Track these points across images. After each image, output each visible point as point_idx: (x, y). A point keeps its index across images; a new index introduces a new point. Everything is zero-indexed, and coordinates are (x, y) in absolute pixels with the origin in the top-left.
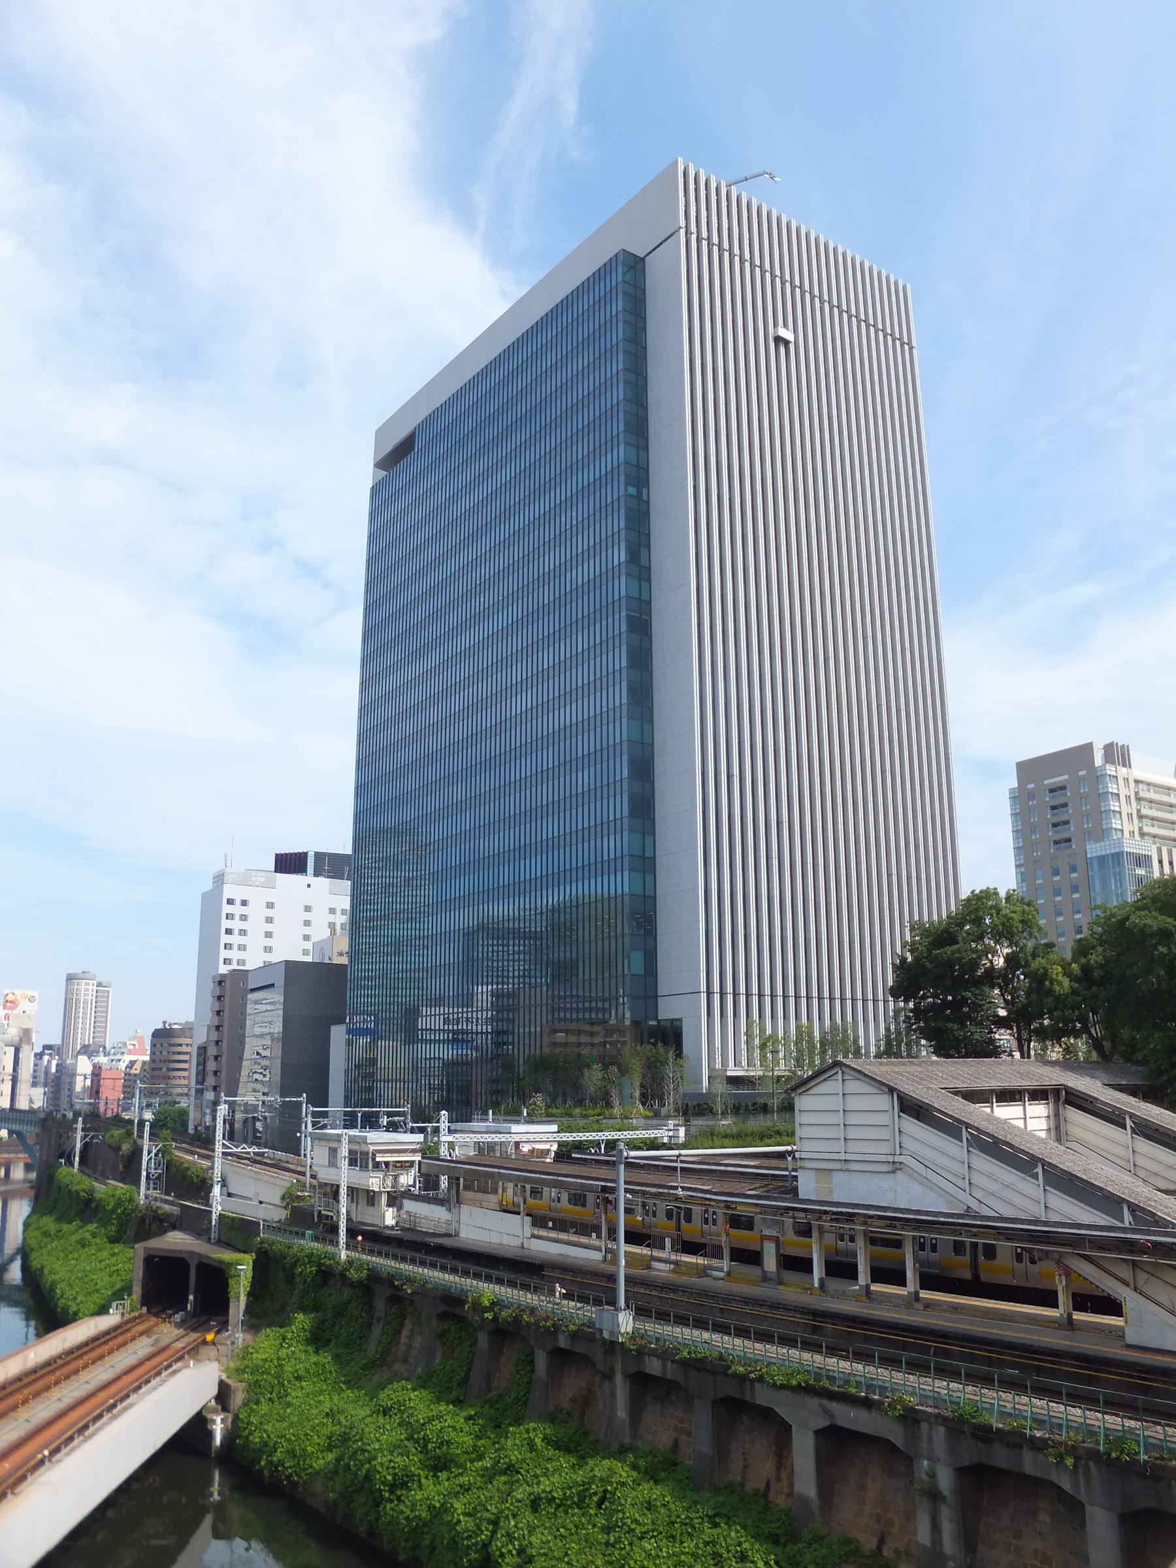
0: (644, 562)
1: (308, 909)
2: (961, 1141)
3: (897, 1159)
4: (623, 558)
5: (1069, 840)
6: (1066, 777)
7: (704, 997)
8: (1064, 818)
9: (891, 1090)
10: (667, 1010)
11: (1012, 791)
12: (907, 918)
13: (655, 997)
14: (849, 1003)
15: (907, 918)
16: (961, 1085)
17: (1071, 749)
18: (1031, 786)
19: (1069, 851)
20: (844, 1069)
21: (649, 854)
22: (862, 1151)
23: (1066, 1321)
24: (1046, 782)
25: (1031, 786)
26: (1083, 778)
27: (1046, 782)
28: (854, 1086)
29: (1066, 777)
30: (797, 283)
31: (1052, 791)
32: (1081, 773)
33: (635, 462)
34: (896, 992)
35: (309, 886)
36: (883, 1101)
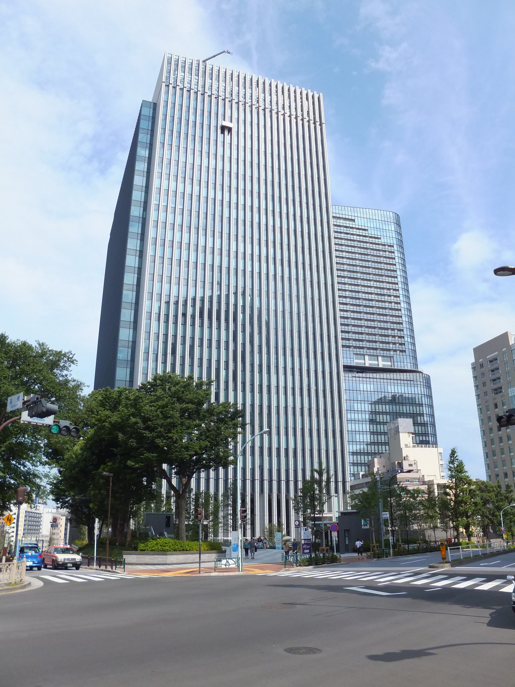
6: (497, 353)
8: (497, 375)
11: (473, 364)
12: (300, 477)
15: (300, 477)
16: (434, 656)
17: (498, 337)
18: (481, 360)
19: (501, 394)
23: (101, 562)
24: (488, 357)
25: (481, 360)
26: (505, 353)
27: (488, 357)
29: (497, 353)
31: (491, 361)
32: (504, 349)
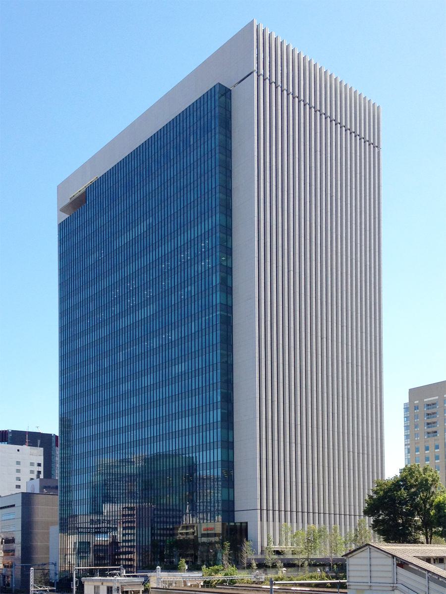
0: (229, 284)
1: (18, 463)
2: (425, 578)
3: (395, 585)
4: (218, 282)
5: (436, 432)
6: (437, 397)
7: (259, 511)
9: (393, 556)
10: (239, 518)
13: (233, 511)
14: (265, 512)
20: (370, 547)
21: (230, 440)
22: (358, 581)
28: (375, 554)
29: (437, 397)
30: (274, 80)
33: (225, 226)
34: (366, 513)
35: (18, 450)
36: (390, 561)
